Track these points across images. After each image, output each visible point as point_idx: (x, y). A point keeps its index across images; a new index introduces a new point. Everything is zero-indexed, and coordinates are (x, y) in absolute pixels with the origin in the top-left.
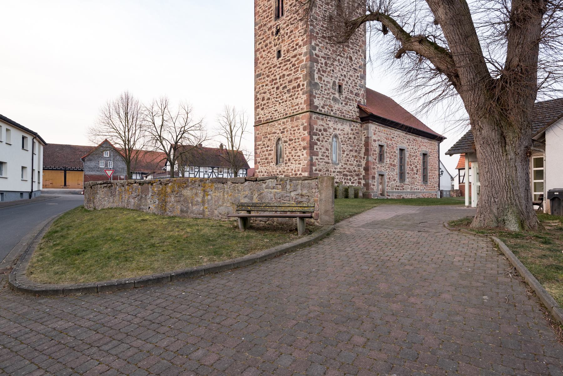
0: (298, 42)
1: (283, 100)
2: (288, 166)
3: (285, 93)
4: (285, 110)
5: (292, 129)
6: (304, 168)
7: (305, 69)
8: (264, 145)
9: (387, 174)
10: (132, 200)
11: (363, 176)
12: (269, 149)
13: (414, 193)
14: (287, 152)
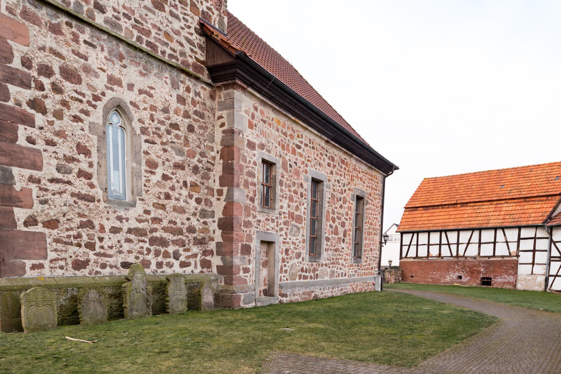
9: (281, 239)
13: (337, 283)
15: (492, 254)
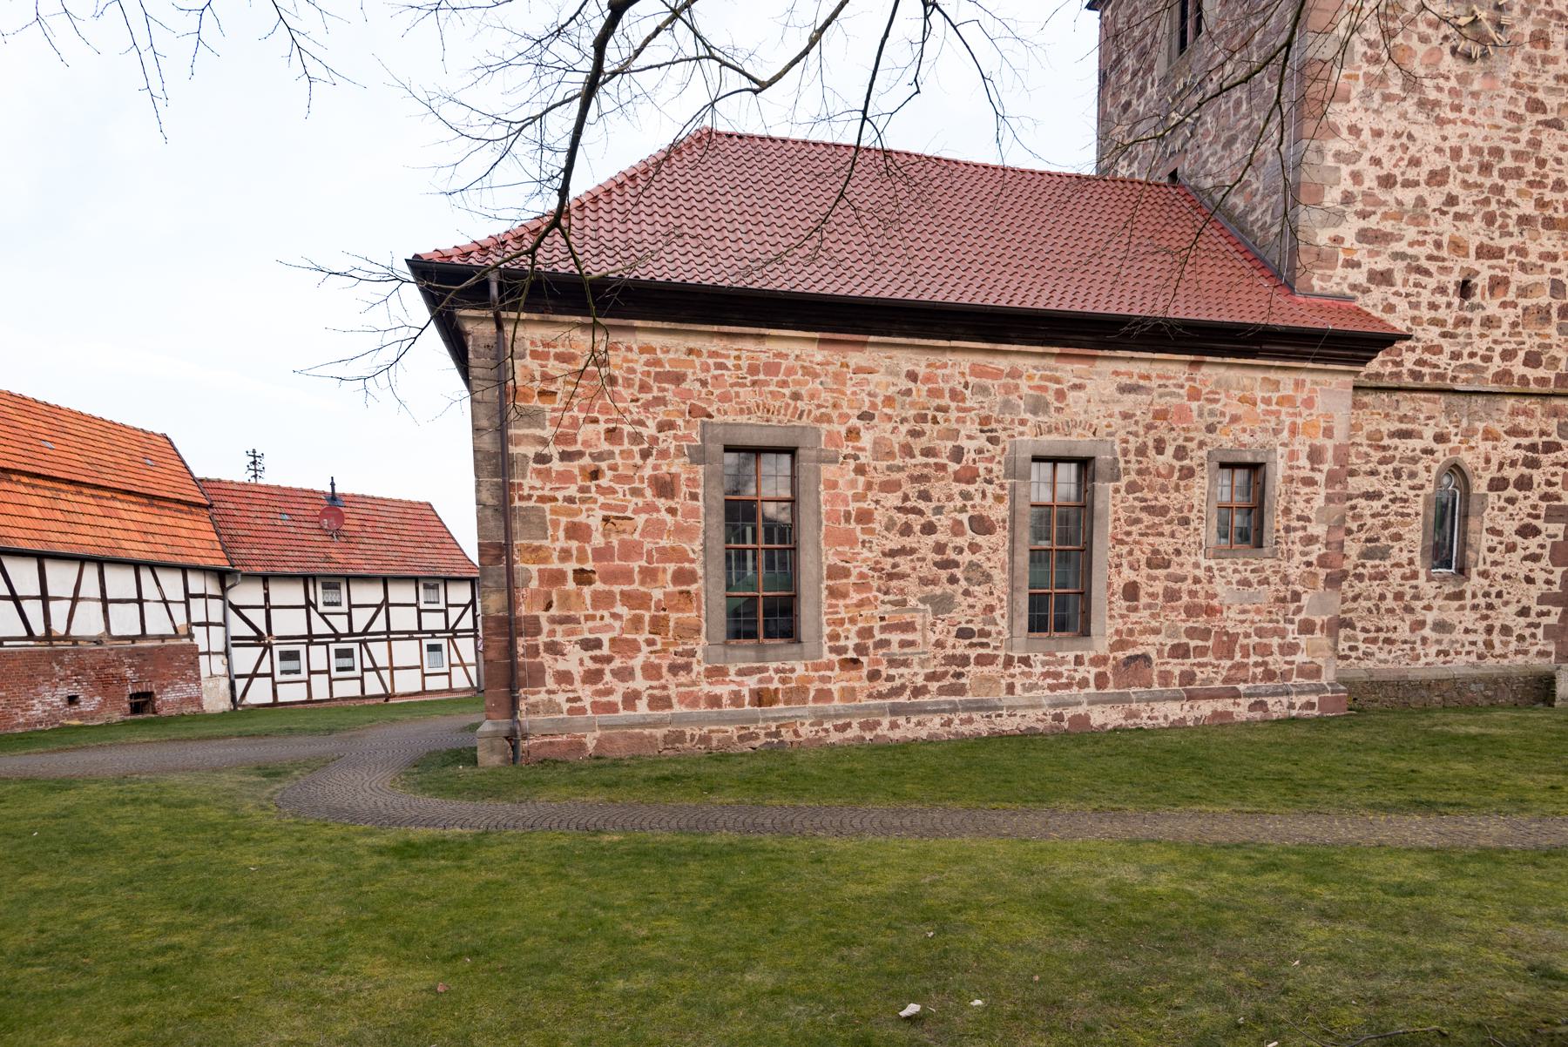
15: (139, 632)
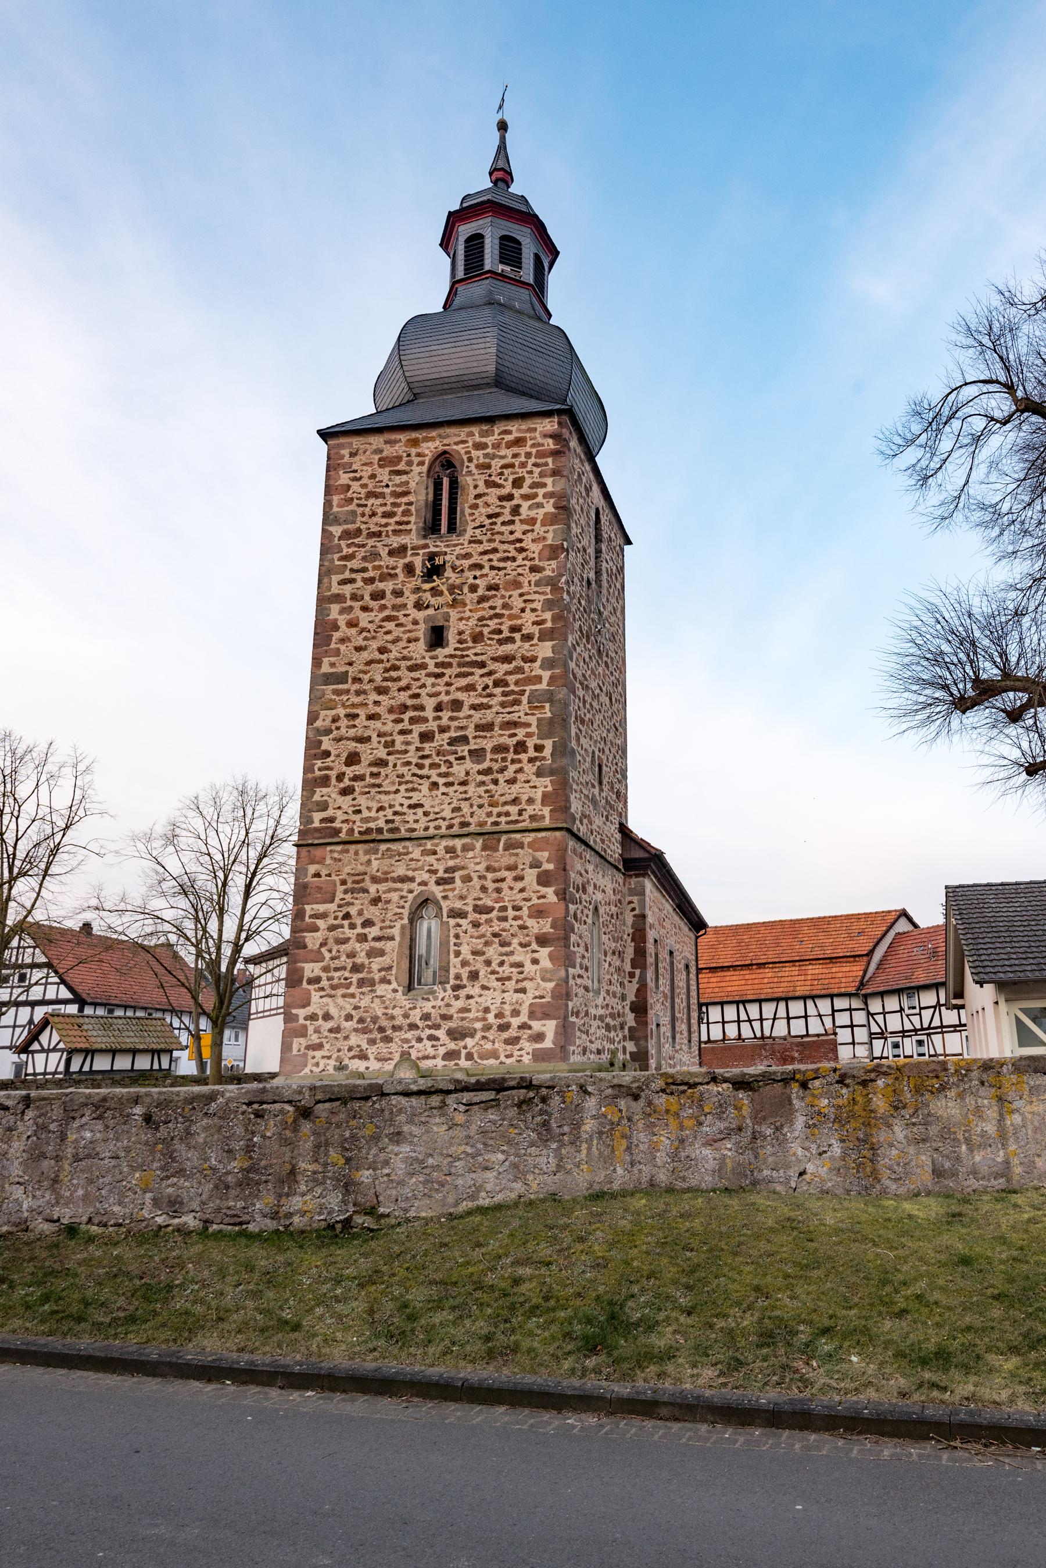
0: (519, 622)
1: (451, 779)
2: (469, 997)
3: (463, 758)
4: (458, 809)
5: (490, 876)
6: (542, 1005)
7: (547, 705)
8: (347, 916)
10: (707, 1152)
11: (630, 1028)
12: (373, 932)
14: (465, 950)
